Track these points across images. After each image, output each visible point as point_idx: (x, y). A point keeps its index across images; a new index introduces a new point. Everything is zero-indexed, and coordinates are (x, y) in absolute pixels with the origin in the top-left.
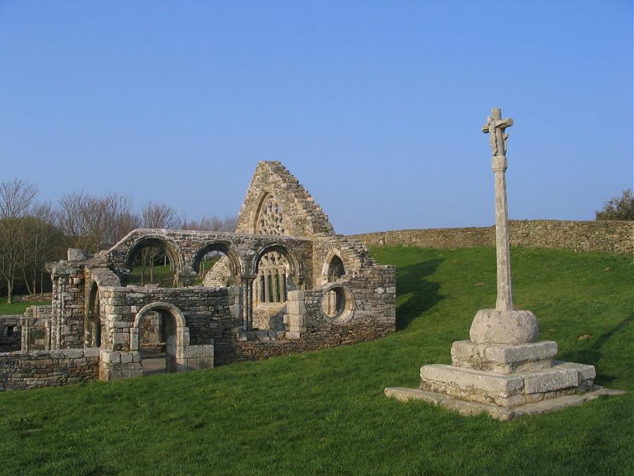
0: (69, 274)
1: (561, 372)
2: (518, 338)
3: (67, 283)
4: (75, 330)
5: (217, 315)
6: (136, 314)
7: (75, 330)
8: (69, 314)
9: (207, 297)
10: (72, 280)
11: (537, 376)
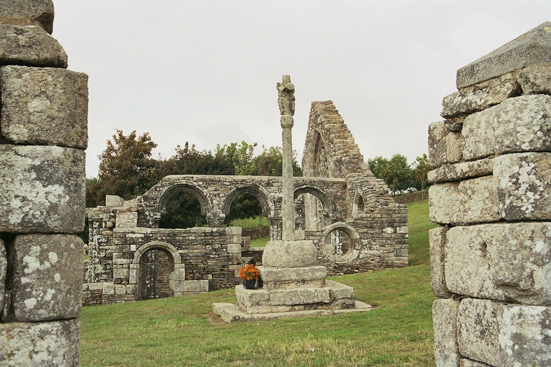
0: (102, 219)
1: (309, 289)
2: (284, 263)
3: (100, 226)
4: (109, 269)
5: (214, 253)
6: (135, 252)
7: (109, 269)
8: (103, 255)
9: (204, 236)
10: (106, 223)
11: (282, 292)
